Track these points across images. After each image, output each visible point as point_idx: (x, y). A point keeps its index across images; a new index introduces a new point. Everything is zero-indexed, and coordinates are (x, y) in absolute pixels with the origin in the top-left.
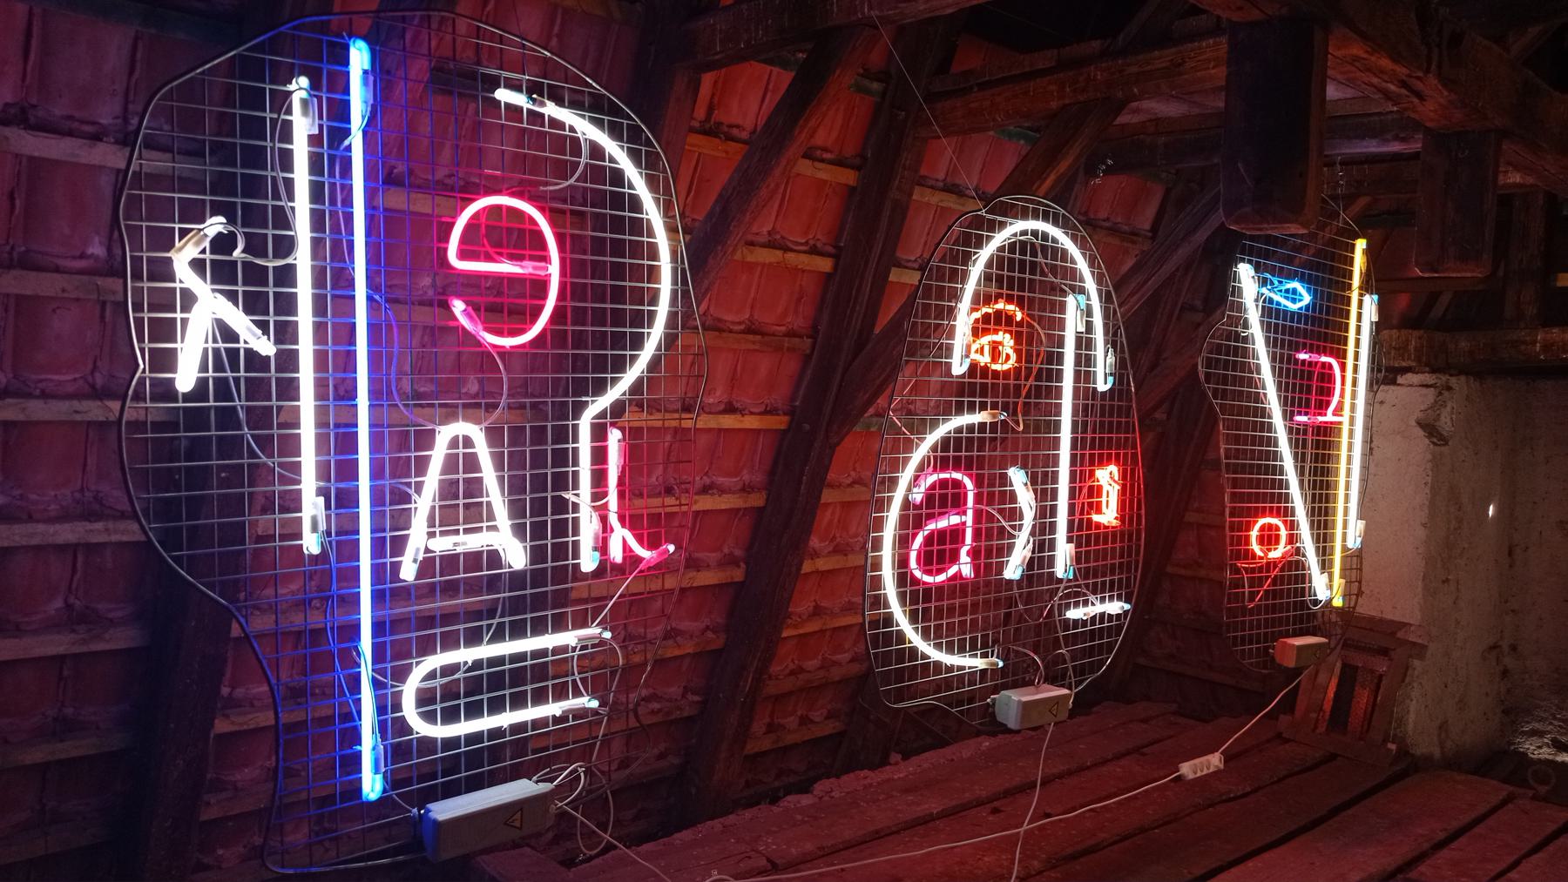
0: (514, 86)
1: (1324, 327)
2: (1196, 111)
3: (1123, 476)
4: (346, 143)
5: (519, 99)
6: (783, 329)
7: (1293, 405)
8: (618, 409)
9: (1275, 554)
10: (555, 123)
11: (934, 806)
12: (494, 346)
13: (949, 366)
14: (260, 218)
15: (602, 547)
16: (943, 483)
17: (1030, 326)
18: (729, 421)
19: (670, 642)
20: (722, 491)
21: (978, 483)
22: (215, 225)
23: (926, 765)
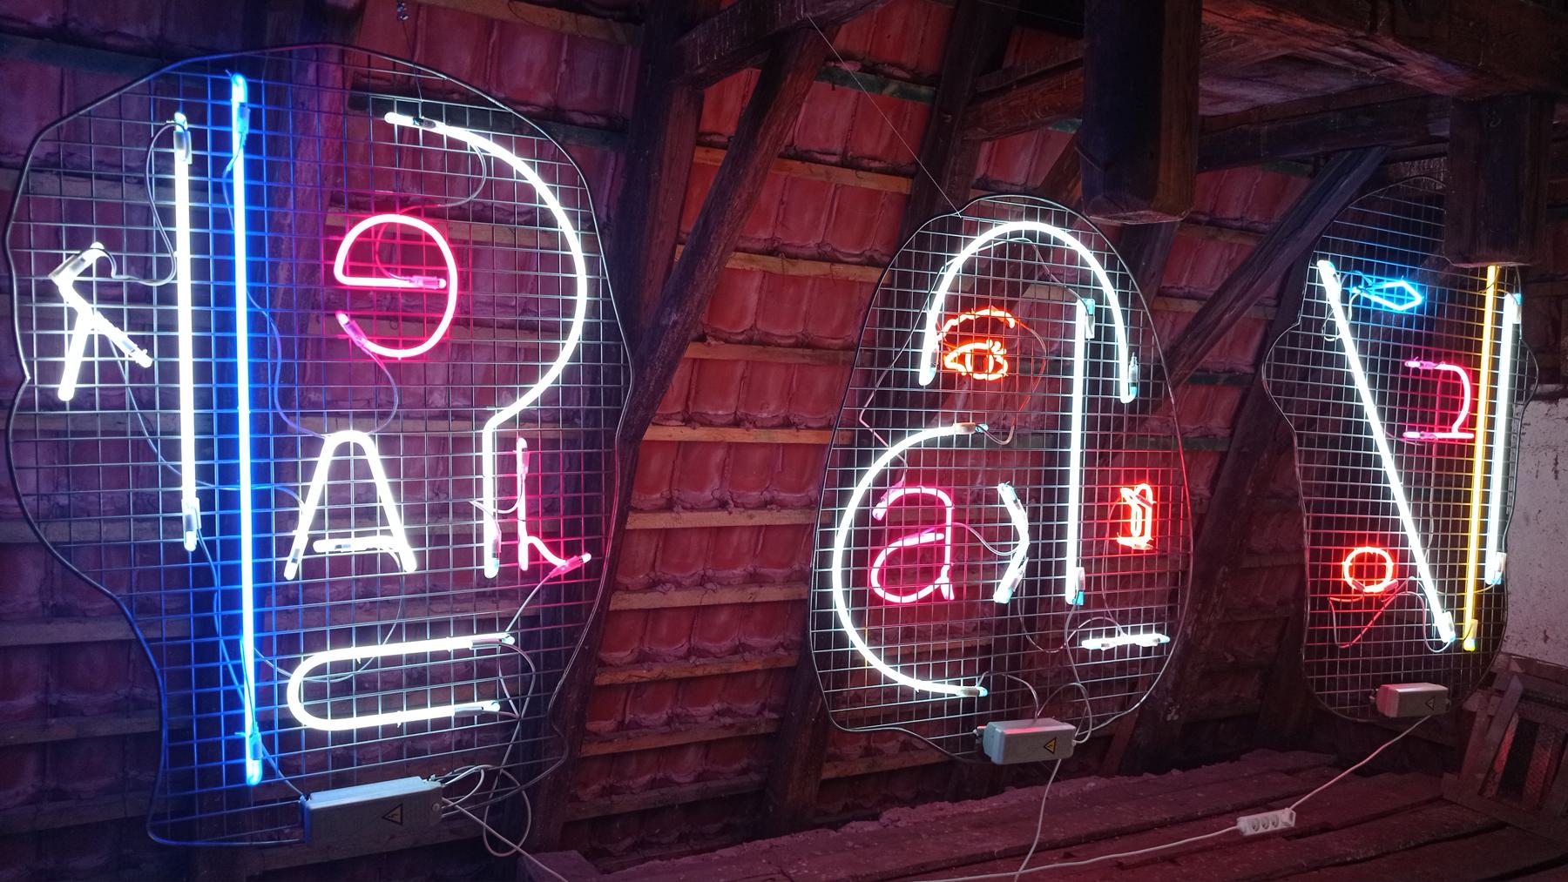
0: (405, 109)
1: (1451, 328)
2: (1296, 96)
3: (1161, 496)
4: (228, 168)
5: (407, 121)
6: (839, 342)
7: (1402, 419)
8: (526, 417)
9: (1375, 589)
10: (453, 143)
11: (997, 845)
12: (381, 357)
13: (915, 376)
14: (140, 244)
15: (507, 553)
16: (911, 500)
17: (1025, 332)
18: (782, 437)
19: (737, 657)
20: (782, 506)
21: (957, 500)
22: (94, 253)
23: (1013, 802)
